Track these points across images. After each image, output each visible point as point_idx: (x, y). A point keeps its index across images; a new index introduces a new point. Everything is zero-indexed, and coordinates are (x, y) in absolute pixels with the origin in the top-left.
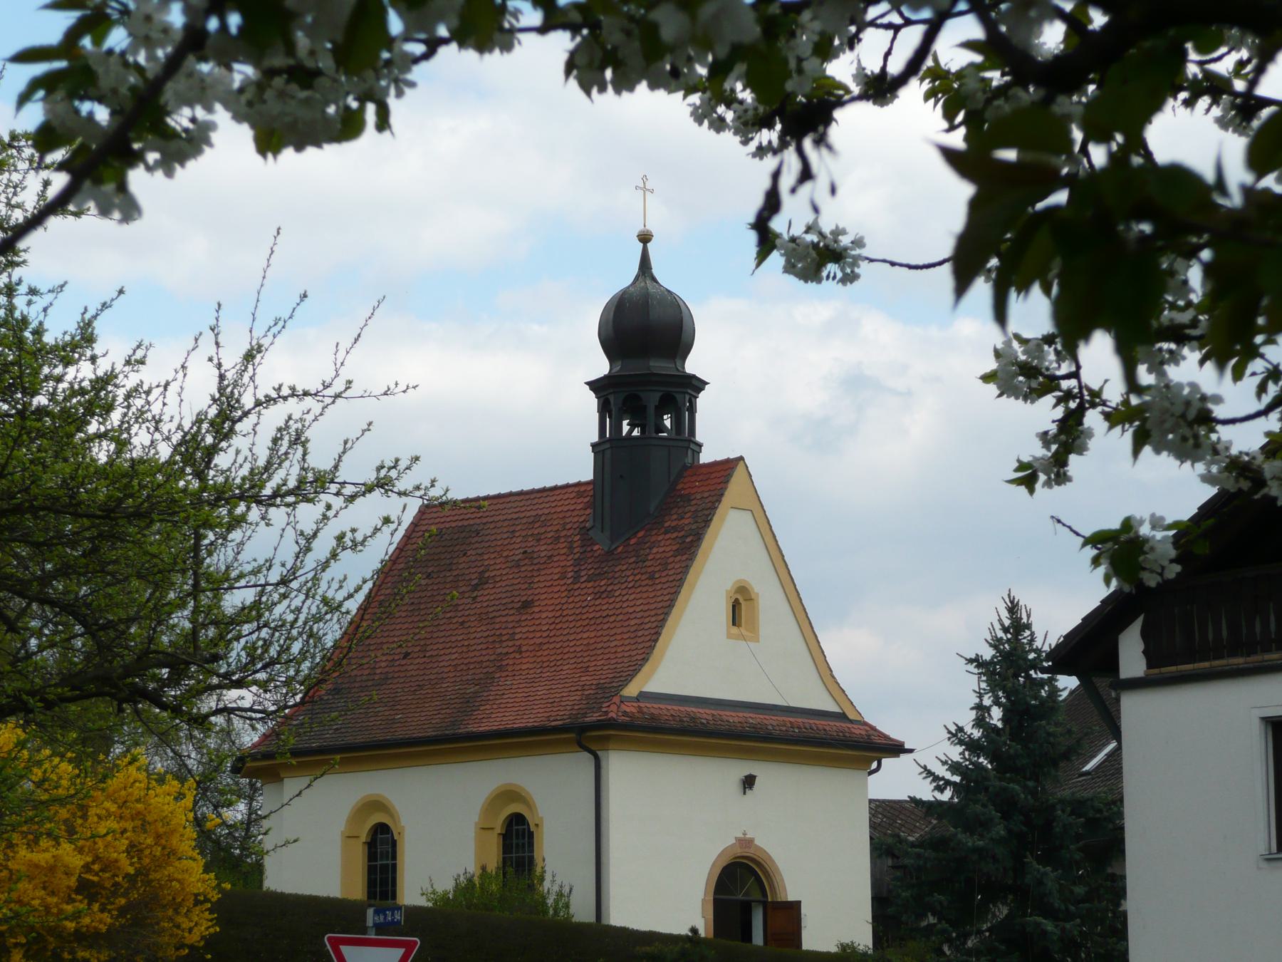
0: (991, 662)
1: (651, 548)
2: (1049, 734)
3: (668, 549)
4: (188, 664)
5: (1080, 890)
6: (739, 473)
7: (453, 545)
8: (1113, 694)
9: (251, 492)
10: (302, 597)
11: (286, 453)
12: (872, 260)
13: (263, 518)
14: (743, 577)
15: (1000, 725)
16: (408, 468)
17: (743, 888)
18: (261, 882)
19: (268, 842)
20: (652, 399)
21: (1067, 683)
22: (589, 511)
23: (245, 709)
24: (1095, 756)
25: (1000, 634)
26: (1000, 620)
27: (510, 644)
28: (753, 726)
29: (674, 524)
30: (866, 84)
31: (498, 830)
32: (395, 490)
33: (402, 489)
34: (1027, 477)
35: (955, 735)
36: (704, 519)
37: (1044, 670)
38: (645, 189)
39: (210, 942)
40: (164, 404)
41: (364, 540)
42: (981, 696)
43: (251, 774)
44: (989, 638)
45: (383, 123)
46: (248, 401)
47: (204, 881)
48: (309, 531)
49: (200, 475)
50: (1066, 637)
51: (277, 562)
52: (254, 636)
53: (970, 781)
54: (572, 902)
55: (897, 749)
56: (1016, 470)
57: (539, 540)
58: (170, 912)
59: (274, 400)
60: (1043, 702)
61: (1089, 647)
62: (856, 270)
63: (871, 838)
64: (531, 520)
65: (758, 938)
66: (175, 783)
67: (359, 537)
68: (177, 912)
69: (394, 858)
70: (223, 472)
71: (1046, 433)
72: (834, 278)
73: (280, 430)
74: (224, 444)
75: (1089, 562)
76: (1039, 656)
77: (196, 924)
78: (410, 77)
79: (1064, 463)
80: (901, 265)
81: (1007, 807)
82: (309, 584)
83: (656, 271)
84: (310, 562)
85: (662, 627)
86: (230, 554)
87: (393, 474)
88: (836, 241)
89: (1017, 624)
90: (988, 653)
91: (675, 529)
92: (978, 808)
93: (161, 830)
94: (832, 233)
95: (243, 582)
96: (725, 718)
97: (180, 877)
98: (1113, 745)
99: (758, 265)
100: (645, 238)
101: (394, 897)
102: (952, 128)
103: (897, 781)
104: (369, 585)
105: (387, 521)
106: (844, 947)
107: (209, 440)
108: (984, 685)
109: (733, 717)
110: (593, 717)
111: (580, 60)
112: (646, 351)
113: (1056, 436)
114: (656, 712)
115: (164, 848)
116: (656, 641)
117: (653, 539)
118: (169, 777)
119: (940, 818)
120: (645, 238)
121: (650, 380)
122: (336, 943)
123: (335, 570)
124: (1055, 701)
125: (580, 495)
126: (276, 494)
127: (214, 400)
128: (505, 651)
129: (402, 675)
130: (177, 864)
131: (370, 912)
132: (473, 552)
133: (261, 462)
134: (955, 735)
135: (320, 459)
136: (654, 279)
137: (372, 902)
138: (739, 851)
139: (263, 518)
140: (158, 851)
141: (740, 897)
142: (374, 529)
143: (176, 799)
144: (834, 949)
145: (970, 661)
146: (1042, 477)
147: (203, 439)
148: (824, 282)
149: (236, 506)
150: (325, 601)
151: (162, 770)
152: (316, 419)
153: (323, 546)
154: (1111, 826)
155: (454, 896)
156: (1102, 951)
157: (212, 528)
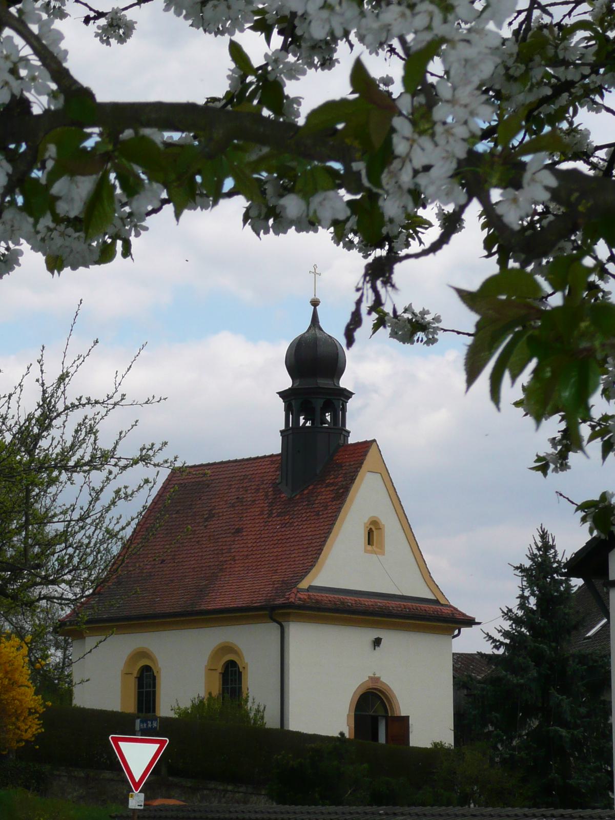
0: (530, 569)
1: (317, 496)
2: (565, 614)
3: (328, 497)
4: (22, 570)
5: (583, 710)
6: (372, 451)
7: (193, 494)
8: (605, 590)
9: (62, 463)
10: (93, 528)
11: (84, 439)
12: (445, 330)
13: (69, 480)
14: (372, 515)
15: (535, 608)
16: (160, 449)
17: (373, 706)
18: (71, 700)
19: (76, 679)
20: (319, 403)
21: (577, 582)
22: (278, 473)
23: (63, 595)
24: (594, 627)
25: (536, 552)
26: (535, 543)
27: (228, 555)
28: (380, 607)
29: (331, 481)
30: (444, 219)
31: (220, 670)
32: (152, 463)
33: (156, 463)
34: (543, 466)
35: (506, 614)
36: (350, 478)
37: (562, 574)
38: (315, 273)
39: (38, 738)
40: (9, 408)
41: (133, 493)
42: (523, 590)
43: (67, 634)
44: (529, 554)
45: (127, 252)
46: (60, 407)
47: (35, 700)
48: (98, 488)
49: (30, 452)
50: (576, 554)
51: (77, 507)
52: (64, 552)
53: (515, 642)
54: (265, 716)
55: (470, 622)
56: (536, 462)
57: (246, 490)
58: (14, 719)
59: (77, 406)
60: (561, 593)
61: (589, 562)
62: (436, 336)
63: (454, 677)
64: (242, 478)
65: (382, 739)
66: (17, 639)
67: (129, 491)
68: (18, 719)
69: (154, 686)
70: (45, 450)
71: (554, 439)
72: (422, 341)
73: (80, 425)
74: (45, 433)
75: (579, 520)
76: (560, 565)
77: (30, 727)
78: (144, 224)
79: (566, 458)
80: (464, 334)
81: (538, 658)
82: (97, 521)
83: (322, 324)
84: (99, 506)
85: (324, 545)
86: (48, 502)
87: (151, 453)
88: (423, 318)
89: (546, 546)
90: (528, 564)
91: (332, 484)
92: (521, 660)
93: (9, 669)
94: (420, 313)
95: (56, 519)
96: (363, 602)
97: (20, 697)
98: (605, 620)
99: (374, 333)
100: (315, 303)
101: (154, 711)
102: (490, 255)
103: (470, 642)
104: (133, 524)
105: (147, 481)
106: (436, 745)
107: (36, 430)
108: (525, 583)
109: (368, 602)
110: (281, 601)
111: (253, 213)
112: (315, 373)
113: (560, 441)
114: (320, 598)
115: (10, 679)
116: (320, 554)
117: (319, 490)
118: (13, 635)
119: (496, 665)
120: (315, 303)
121: (318, 391)
122: (116, 741)
123: (114, 512)
124: (569, 593)
125: (273, 462)
126: (77, 464)
127: (39, 406)
128: (225, 559)
129: (160, 573)
130: (18, 690)
131: (138, 721)
132: (205, 498)
133: (68, 444)
134: (506, 614)
135: (105, 443)
136: (321, 329)
137: (140, 714)
138: (371, 685)
139: (69, 480)
140: (6, 682)
141: (371, 713)
142: (141, 486)
143: (18, 649)
144: (429, 746)
145: (517, 568)
146: (552, 466)
147: (32, 431)
148: (415, 343)
149: (52, 473)
150: (108, 531)
151: (9, 632)
152: (102, 418)
153: (107, 497)
154: (603, 670)
155: (192, 711)
156: (597, 748)
157: (36, 486)
